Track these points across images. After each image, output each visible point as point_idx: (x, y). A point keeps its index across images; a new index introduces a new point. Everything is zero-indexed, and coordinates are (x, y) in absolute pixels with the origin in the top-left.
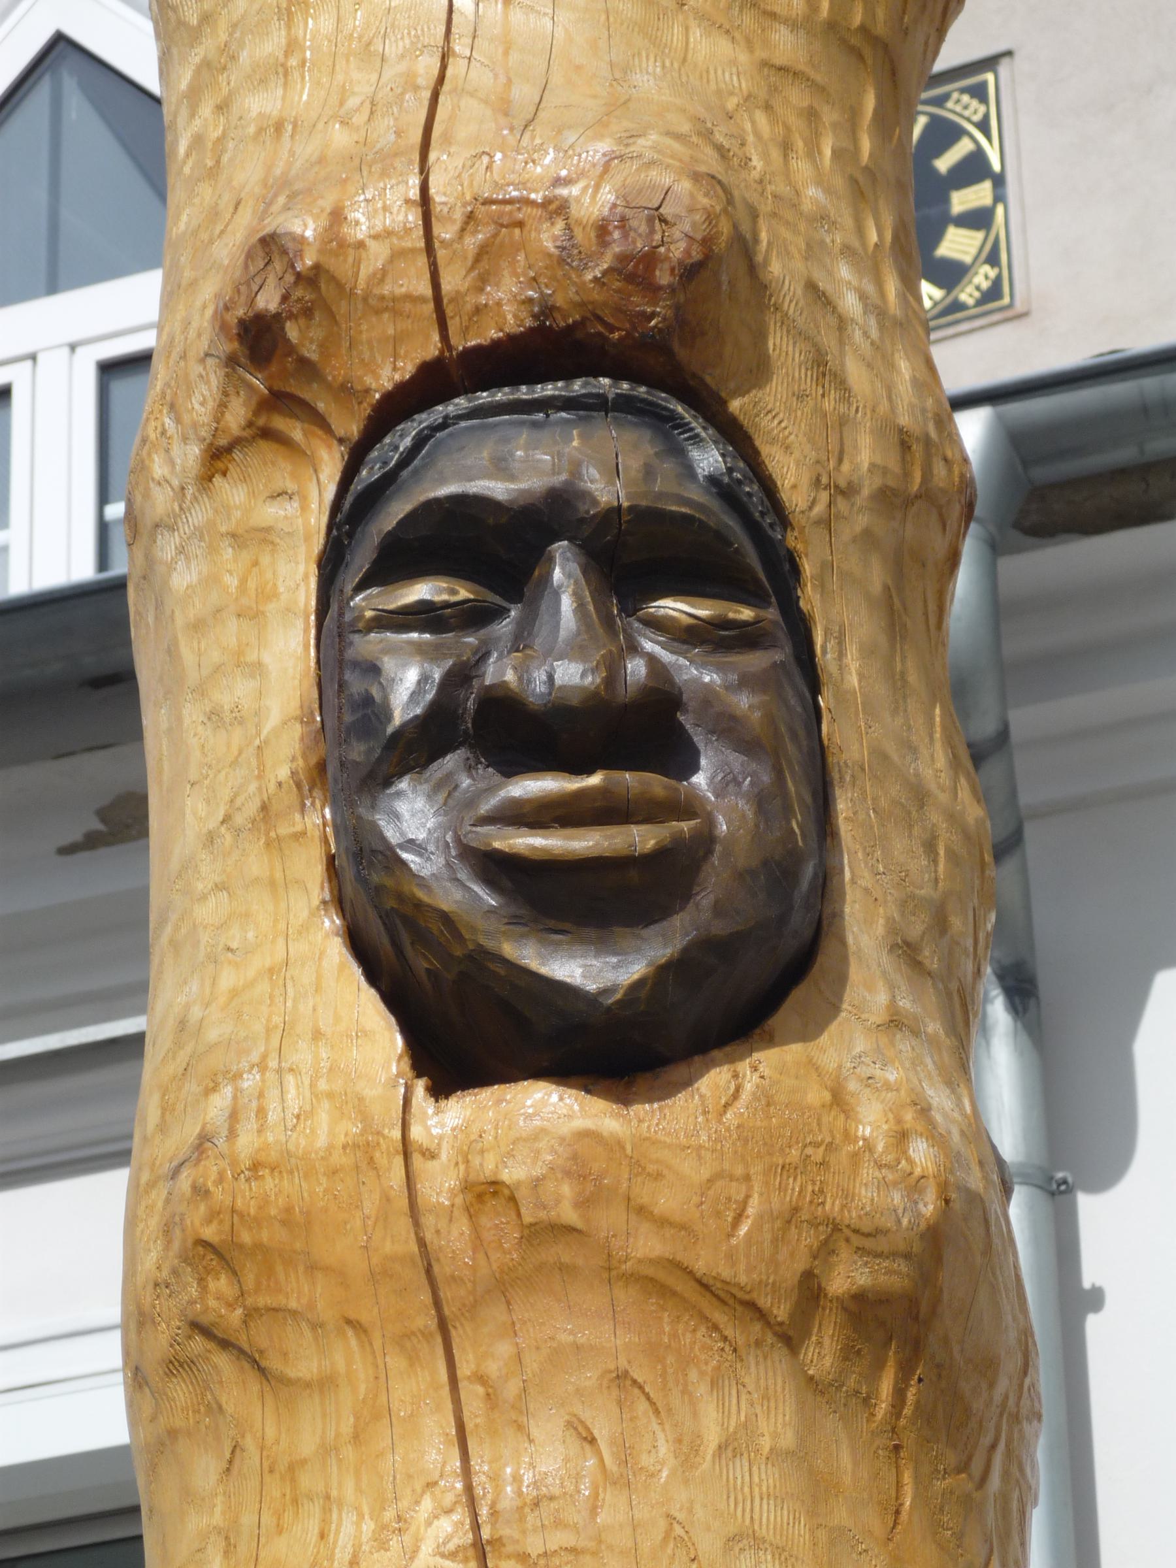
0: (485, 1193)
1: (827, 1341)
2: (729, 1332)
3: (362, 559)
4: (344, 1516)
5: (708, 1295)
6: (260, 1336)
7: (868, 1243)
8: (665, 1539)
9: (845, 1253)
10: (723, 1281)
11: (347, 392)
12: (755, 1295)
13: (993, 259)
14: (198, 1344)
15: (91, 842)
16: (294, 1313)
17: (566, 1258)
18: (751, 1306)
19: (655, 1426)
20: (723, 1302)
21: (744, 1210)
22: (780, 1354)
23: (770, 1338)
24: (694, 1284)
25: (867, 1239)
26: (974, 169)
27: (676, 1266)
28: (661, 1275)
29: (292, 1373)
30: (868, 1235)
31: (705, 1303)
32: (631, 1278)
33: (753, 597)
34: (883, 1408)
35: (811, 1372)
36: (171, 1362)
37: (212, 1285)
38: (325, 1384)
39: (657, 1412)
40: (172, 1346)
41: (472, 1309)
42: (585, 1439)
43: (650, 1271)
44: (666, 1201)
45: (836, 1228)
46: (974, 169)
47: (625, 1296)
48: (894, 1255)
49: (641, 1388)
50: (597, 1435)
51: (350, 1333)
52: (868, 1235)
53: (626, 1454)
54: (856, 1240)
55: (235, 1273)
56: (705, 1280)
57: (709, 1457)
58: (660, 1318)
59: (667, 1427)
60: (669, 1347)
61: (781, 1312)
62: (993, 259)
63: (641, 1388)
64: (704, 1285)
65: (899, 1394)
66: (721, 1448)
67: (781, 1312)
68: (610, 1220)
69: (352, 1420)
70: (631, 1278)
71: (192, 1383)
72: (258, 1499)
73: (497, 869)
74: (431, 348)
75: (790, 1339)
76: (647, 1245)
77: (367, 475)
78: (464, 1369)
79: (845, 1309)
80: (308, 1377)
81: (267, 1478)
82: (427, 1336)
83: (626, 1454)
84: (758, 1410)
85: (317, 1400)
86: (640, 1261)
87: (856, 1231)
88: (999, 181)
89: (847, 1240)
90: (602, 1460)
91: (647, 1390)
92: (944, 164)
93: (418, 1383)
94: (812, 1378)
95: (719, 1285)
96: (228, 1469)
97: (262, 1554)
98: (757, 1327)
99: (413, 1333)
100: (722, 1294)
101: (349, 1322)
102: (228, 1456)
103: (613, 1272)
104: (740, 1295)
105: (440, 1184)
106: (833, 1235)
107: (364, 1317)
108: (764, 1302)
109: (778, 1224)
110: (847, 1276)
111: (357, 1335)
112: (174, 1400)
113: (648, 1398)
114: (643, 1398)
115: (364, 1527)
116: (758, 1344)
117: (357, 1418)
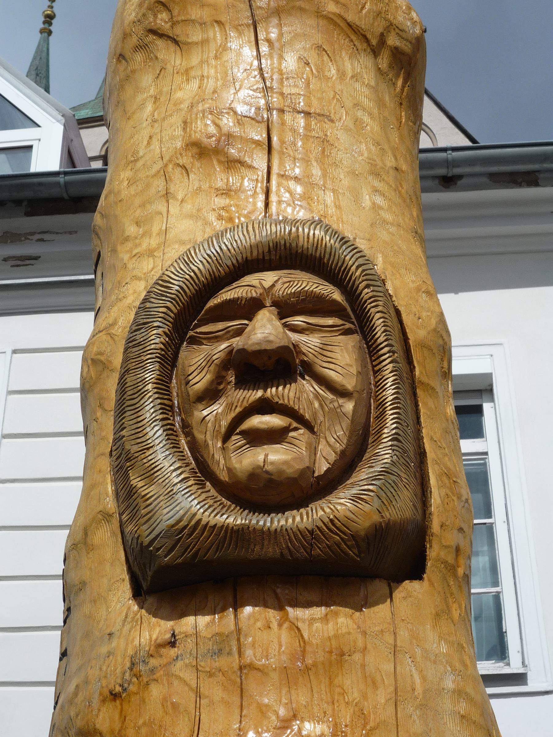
1: (385, 59)
2: (356, 43)
4: (210, 80)
5: (350, 29)
6: (178, 31)
7: (400, 33)
8: (333, 98)
9: (393, 33)
10: (357, 25)
12: (366, 33)
14: (151, 37)
16: (193, 21)
17: (303, 6)
18: (365, 36)
19: (330, 64)
20: (355, 32)
21: (364, 6)
22: (371, 56)
23: (369, 50)
24: (346, 24)
25: (400, 31)
27: (340, 16)
28: (335, 19)
29: (190, 41)
30: (401, 30)
31: (349, 32)
32: (326, 17)
34: (398, 89)
35: (380, 66)
36: (137, 47)
37: (159, 16)
38: (205, 42)
39: (331, 61)
40: (138, 41)
41: (267, 19)
42: (305, 63)
43: (331, 16)
45: (391, 24)
47: (322, 22)
48: (407, 40)
49: (326, 52)
50: (310, 61)
51: (216, 25)
52: (401, 30)
53: (320, 70)
54: (397, 30)
55: (170, 11)
56: (350, 24)
57: (348, 78)
58: (334, 33)
59: (334, 65)
60: (336, 41)
61: (374, 42)
63: (326, 52)
64: (349, 25)
65: (403, 87)
66: (352, 77)
67: (374, 42)
69: (215, 52)
70: (326, 17)
71: (145, 53)
72: (171, 84)
75: (375, 52)
78: (261, 36)
79: (392, 51)
80: (197, 41)
81: (175, 75)
82: (248, 26)
83: (320, 70)
84: (364, 71)
85: (200, 48)
86: (328, 12)
87: (397, 27)
89: (394, 29)
90: (312, 70)
91: (328, 52)
93: (242, 40)
94: (380, 68)
95: (355, 26)
96: (158, 77)
97: (172, 97)
98: (365, 44)
99: (242, 25)
100: (356, 30)
101: (216, 22)
102: (158, 72)
103: (319, 14)
104: (361, 31)
106: (390, 26)
107: (223, 20)
108: (369, 36)
109: (375, 14)
110: (392, 40)
111: (219, 26)
112: (136, 60)
113: (328, 56)
114: (326, 55)
115: (219, 83)
116: (365, 50)
117: (217, 51)
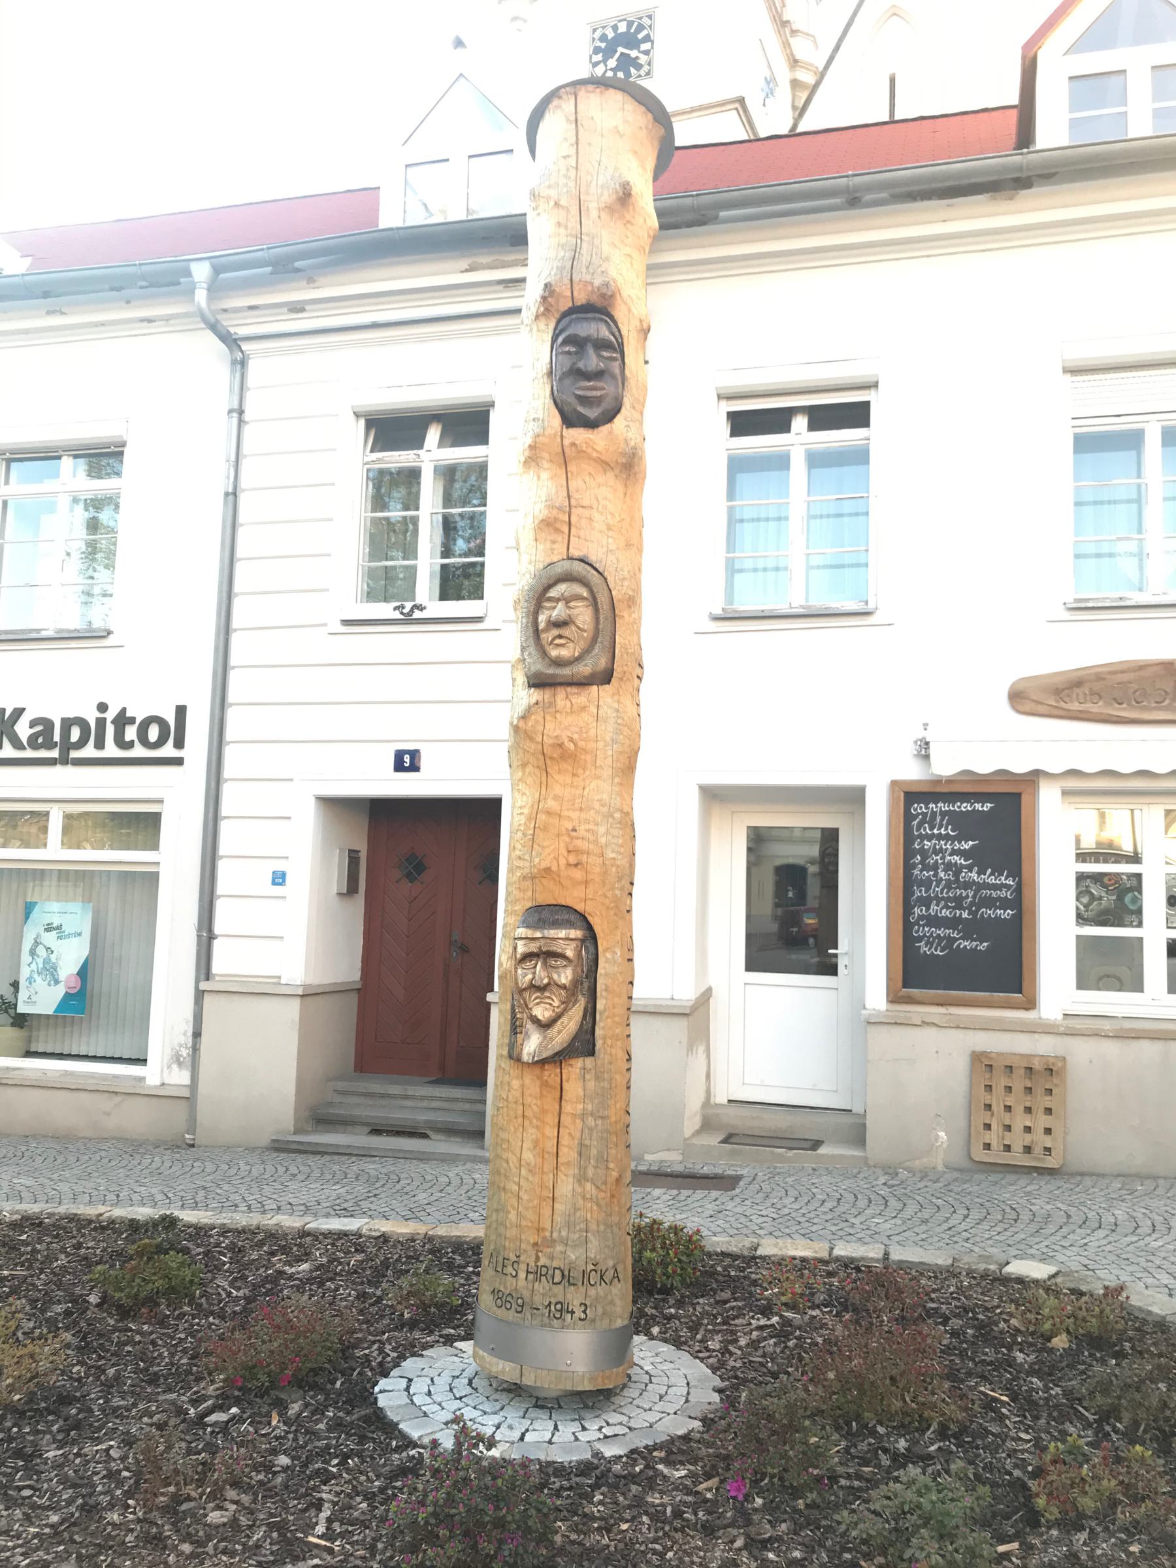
0: (573, 444)
3: (560, 339)
11: (557, 311)
13: (649, 64)
15: (467, 271)
26: (647, 39)
33: (615, 350)
44: (598, 448)
46: (647, 39)
47: (591, 462)
62: (649, 64)
68: (589, 450)
73: (579, 397)
74: (570, 305)
76: (595, 455)
77: (560, 327)
88: (652, 42)
92: (640, 36)
105: (566, 442)
